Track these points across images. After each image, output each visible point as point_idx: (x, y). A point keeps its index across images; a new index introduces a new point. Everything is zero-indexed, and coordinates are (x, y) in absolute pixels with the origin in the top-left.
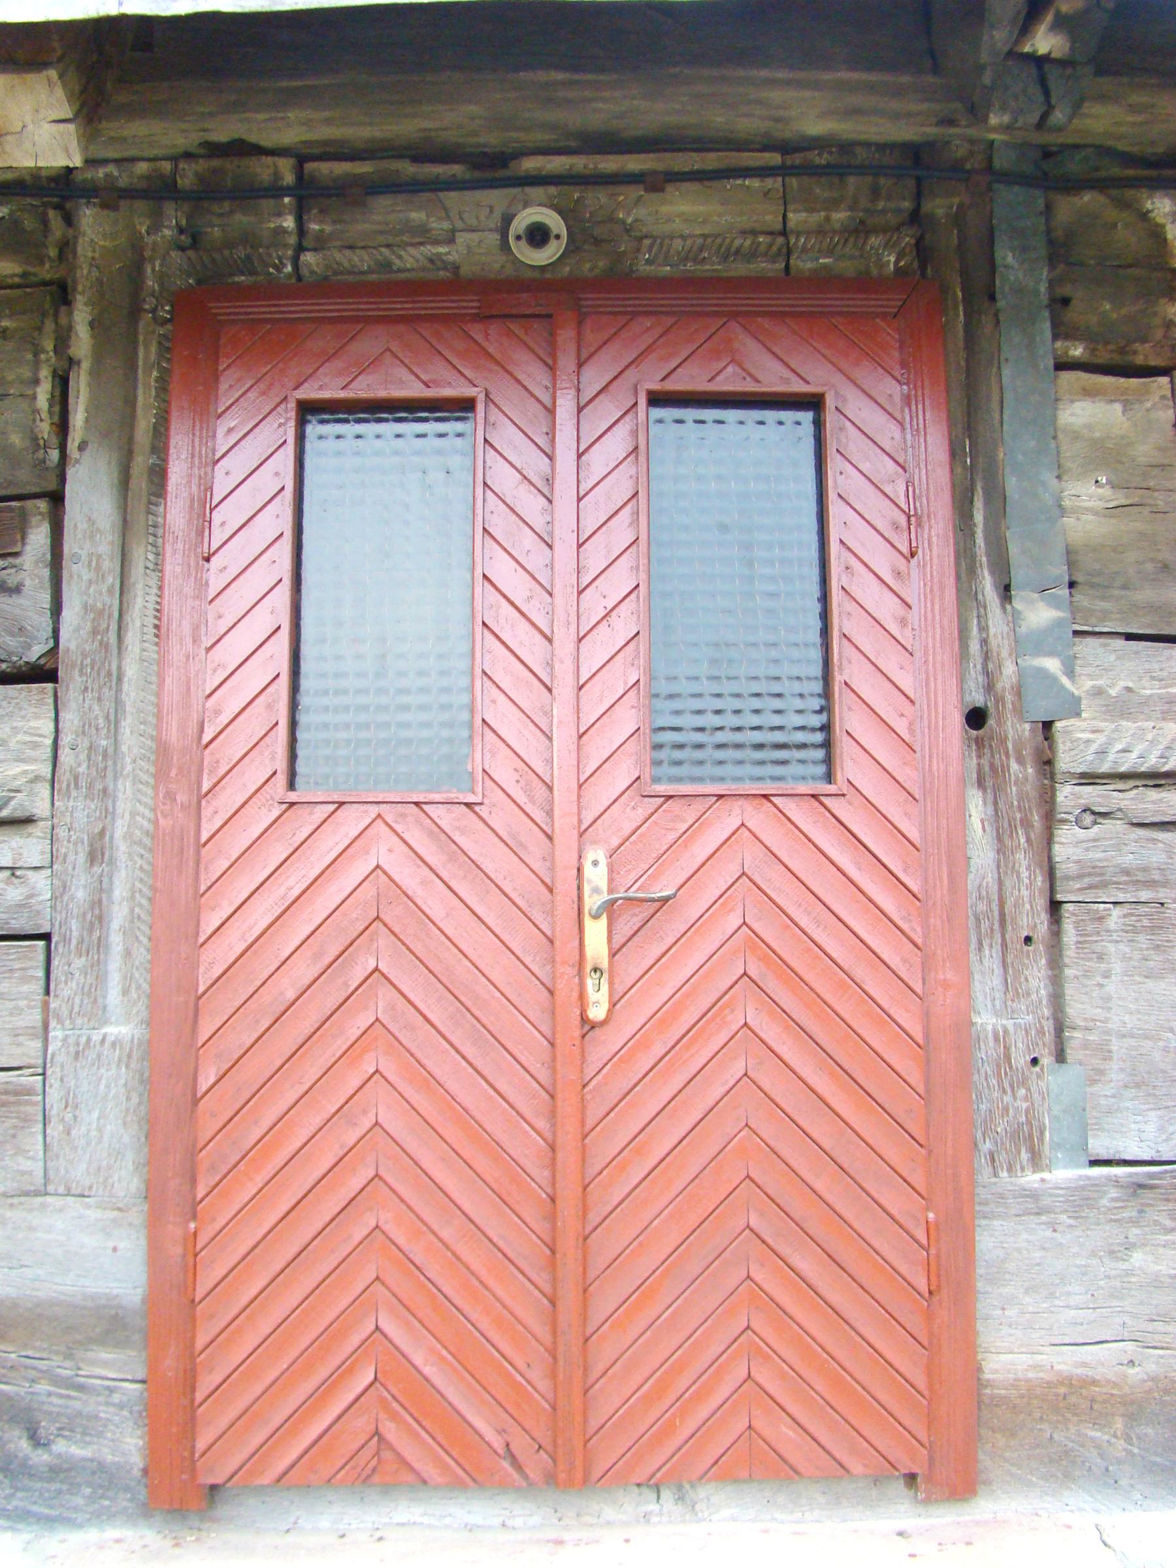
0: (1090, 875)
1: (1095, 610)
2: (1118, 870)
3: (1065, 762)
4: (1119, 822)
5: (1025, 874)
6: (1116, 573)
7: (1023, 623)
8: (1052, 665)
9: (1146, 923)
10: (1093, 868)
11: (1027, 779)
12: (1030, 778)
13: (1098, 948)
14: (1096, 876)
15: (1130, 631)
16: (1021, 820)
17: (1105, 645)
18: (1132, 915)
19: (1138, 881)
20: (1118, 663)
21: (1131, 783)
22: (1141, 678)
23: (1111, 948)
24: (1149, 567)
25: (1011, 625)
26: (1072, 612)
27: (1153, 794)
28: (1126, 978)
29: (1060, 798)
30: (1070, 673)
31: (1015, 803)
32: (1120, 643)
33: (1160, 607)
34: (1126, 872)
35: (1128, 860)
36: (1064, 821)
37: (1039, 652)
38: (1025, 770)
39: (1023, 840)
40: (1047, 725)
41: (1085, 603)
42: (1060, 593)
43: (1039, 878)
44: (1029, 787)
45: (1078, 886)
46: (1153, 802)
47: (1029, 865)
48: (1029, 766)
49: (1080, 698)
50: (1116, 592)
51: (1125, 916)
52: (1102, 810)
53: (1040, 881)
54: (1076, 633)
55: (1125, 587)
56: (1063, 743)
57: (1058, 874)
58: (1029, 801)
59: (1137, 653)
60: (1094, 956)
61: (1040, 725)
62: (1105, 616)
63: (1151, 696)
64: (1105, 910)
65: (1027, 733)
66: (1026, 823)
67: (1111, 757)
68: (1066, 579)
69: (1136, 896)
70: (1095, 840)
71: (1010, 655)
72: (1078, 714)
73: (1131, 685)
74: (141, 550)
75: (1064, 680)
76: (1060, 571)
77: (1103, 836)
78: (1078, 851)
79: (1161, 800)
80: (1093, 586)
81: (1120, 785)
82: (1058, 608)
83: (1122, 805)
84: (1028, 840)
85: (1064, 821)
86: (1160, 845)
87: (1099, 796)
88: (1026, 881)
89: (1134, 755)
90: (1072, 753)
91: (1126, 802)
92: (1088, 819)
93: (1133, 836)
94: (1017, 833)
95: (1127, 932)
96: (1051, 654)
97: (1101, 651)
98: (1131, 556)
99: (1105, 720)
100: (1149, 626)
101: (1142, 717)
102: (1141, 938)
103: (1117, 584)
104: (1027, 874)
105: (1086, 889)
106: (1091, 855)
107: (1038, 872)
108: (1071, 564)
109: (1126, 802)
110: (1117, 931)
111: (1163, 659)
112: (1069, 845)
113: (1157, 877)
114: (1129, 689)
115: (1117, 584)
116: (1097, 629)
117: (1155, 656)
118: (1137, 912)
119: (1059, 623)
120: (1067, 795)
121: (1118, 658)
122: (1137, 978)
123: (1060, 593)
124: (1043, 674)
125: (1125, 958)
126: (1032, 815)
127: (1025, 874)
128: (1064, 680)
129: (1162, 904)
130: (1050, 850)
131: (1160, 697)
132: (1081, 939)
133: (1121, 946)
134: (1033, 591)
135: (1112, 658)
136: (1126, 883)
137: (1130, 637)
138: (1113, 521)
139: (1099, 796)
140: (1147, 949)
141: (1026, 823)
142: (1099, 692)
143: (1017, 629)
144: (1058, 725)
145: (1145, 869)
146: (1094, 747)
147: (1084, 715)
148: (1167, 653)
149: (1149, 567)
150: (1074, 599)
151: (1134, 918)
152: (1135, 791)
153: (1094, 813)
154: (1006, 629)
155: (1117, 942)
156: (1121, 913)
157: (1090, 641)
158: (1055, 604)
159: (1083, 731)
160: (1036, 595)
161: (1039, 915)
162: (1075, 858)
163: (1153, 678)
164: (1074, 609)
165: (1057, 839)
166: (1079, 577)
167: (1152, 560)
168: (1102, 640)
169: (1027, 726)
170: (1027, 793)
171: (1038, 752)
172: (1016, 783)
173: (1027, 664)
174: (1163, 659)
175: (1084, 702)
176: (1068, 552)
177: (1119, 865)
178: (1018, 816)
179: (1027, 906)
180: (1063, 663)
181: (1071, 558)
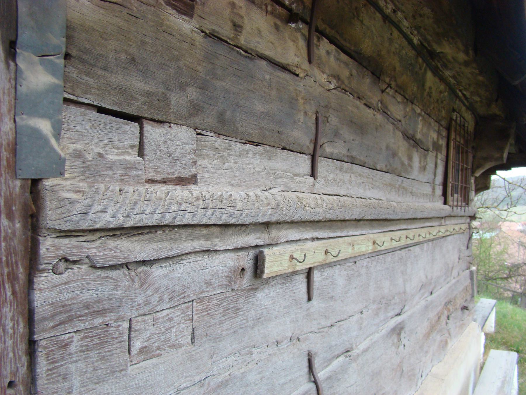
0: (61, 313)
1: (81, 83)
2: (81, 305)
3: (51, 217)
4: (84, 266)
5: (9, 324)
6: (101, 55)
7: (24, 83)
8: (44, 126)
9: (96, 341)
10: (64, 306)
11: (14, 233)
12: (18, 233)
13: (62, 370)
14: (66, 315)
15: (103, 105)
16: (9, 275)
17: (85, 114)
18: (86, 337)
19: (94, 312)
20: (91, 131)
21: (98, 235)
22: (105, 145)
23: (72, 367)
24: (123, 56)
25: (13, 82)
26: (65, 82)
27: (112, 243)
28: (83, 389)
29: (43, 250)
30: (58, 136)
31: (4, 259)
32: (93, 114)
33: (126, 91)
34: (87, 306)
35: (88, 296)
36: (44, 270)
37: (34, 112)
38: (14, 226)
39: (9, 294)
40: (35, 182)
41: (74, 75)
42: (58, 61)
43: (22, 325)
44: (16, 241)
45: (52, 324)
46: (111, 249)
47: (13, 316)
48: (17, 221)
49: (65, 160)
50: (100, 72)
51: (82, 339)
52: (75, 259)
53: (22, 328)
54: (67, 101)
55: (105, 69)
56: (51, 201)
57: (37, 317)
58: (16, 255)
59: (105, 124)
60: (60, 378)
61: (30, 182)
62: (88, 89)
63: (115, 161)
64: (69, 338)
65: (17, 189)
66: (12, 277)
67: (91, 216)
68: (64, 50)
69: (92, 324)
70: (66, 283)
71: (9, 111)
72: (62, 174)
73: (101, 151)
74: (470, 127)
75: (53, 141)
76: (58, 41)
77: (72, 279)
78: (54, 294)
79: (116, 247)
80: (83, 61)
81: (90, 237)
82: (54, 74)
83: (90, 252)
84: (14, 293)
85: (44, 270)
86: (111, 281)
87: (73, 247)
88: (11, 331)
89: (108, 215)
90: (59, 211)
91: (93, 251)
92: (62, 266)
93: (93, 276)
94: (4, 288)
95: (83, 351)
96: (43, 116)
97: (81, 118)
98: (113, 45)
99: (81, 181)
100: (116, 104)
101: (107, 179)
102: (93, 354)
103: (100, 64)
104: (11, 325)
105: (58, 325)
106: (62, 297)
107: (20, 320)
108: (69, 38)
109: (93, 251)
110: (76, 353)
111: (121, 131)
112: (47, 291)
113: (107, 306)
114: (100, 155)
115: (100, 64)
116: (80, 100)
117: (116, 128)
118: (91, 334)
119: (52, 89)
120: (48, 246)
121: (92, 127)
122: (90, 387)
123: (58, 61)
124: (36, 133)
125: (82, 373)
126: (17, 268)
127: (9, 324)
128: (53, 141)
129: (107, 325)
130: (29, 294)
131: (120, 162)
132: (51, 367)
133: (79, 364)
134: (35, 54)
135: (88, 126)
136: (86, 315)
137: (101, 110)
138: (102, 11)
139: (73, 247)
140: (97, 361)
141: (12, 277)
142: (79, 155)
143: (19, 87)
144: (47, 183)
145: (99, 301)
146: (79, 208)
147: (67, 175)
148: (124, 127)
149: (123, 56)
150: (67, 70)
151: (88, 340)
152: (100, 241)
153: (67, 260)
154: (7, 86)
155: (76, 361)
156: (79, 337)
157: (73, 108)
158: (52, 70)
159: (68, 191)
160: (36, 59)
161: (20, 358)
162: (50, 301)
163: (113, 146)
164: (66, 79)
165: (35, 286)
166: (73, 52)
167: (126, 52)
168: (82, 110)
169: (18, 183)
170: (15, 248)
171: (25, 207)
172: (5, 239)
173: (24, 123)
174: (121, 131)
175: (67, 163)
176: (68, 27)
177: (81, 301)
178: (6, 270)
179: (11, 355)
180: (53, 127)
181: (70, 31)
